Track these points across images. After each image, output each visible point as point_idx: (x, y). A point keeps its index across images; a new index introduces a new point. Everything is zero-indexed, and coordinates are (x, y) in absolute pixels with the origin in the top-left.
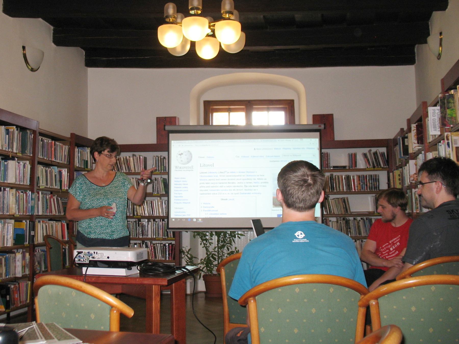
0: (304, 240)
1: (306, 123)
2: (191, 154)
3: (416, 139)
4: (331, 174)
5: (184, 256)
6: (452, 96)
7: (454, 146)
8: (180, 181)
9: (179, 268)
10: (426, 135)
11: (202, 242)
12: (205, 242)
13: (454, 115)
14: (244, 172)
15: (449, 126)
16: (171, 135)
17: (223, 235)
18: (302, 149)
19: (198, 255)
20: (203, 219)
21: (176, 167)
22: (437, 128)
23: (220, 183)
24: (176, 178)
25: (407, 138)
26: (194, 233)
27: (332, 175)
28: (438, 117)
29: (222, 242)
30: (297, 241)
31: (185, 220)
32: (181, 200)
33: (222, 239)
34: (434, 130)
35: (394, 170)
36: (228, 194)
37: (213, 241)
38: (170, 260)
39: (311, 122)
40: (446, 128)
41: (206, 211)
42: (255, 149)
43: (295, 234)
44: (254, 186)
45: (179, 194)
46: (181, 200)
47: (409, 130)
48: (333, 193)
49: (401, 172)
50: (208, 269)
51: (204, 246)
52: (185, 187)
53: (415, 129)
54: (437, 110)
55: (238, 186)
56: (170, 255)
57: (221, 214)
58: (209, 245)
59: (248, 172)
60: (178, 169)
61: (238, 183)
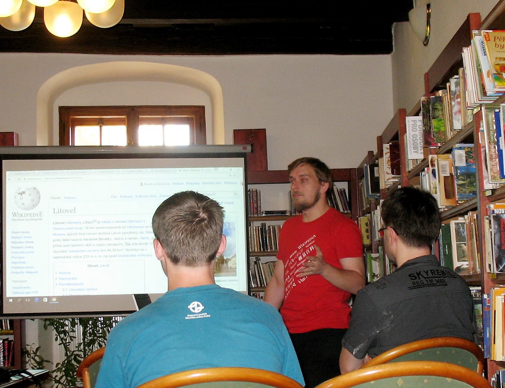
0: (203, 314)
1: (222, 143)
2: (38, 192)
3: (390, 167)
4: (262, 224)
5: (29, 359)
6: (440, 99)
7: (442, 175)
8: (21, 237)
9: (18, 373)
10: (405, 160)
11: (58, 336)
12: (62, 335)
13: (442, 129)
14: (125, 222)
15: (436, 144)
16: (4, 162)
17: (92, 324)
18: (217, 183)
19: (52, 358)
20: (59, 298)
21: (14, 214)
22: (419, 148)
23: (87, 240)
24: (14, 232)
25: (377, 165)
26: (44, 322)
27: (264, 225)
28: (420, 133)
29: (90, 336)
30: (192, 317)
31: (29, 300)
32: (23, 268)
33: (91, 330)
34: (414, 152)
35: (359, 217)
36: (100, 256)
37: (75, 334)
38: (6, 366)
39: (231, 142)
40: (431, 148)
41: (63, 285)
42: (142, 183)
43: (189, 307)
44: (140, 244)
45: (19, 258)
46: (23, 268)
47: (381, 153)
48: (265, 254)
49: (370, 218)
50: (69, 378)
51: (61, 342)
52: (30, 247)
53: (389, 151)
54: (419, 121)
55: (115, 245)
56: (7, 358)
57: (88, 290)
58: (70, 341)
59: (131, 221)
60: (17, 218)
61: (116, 239)
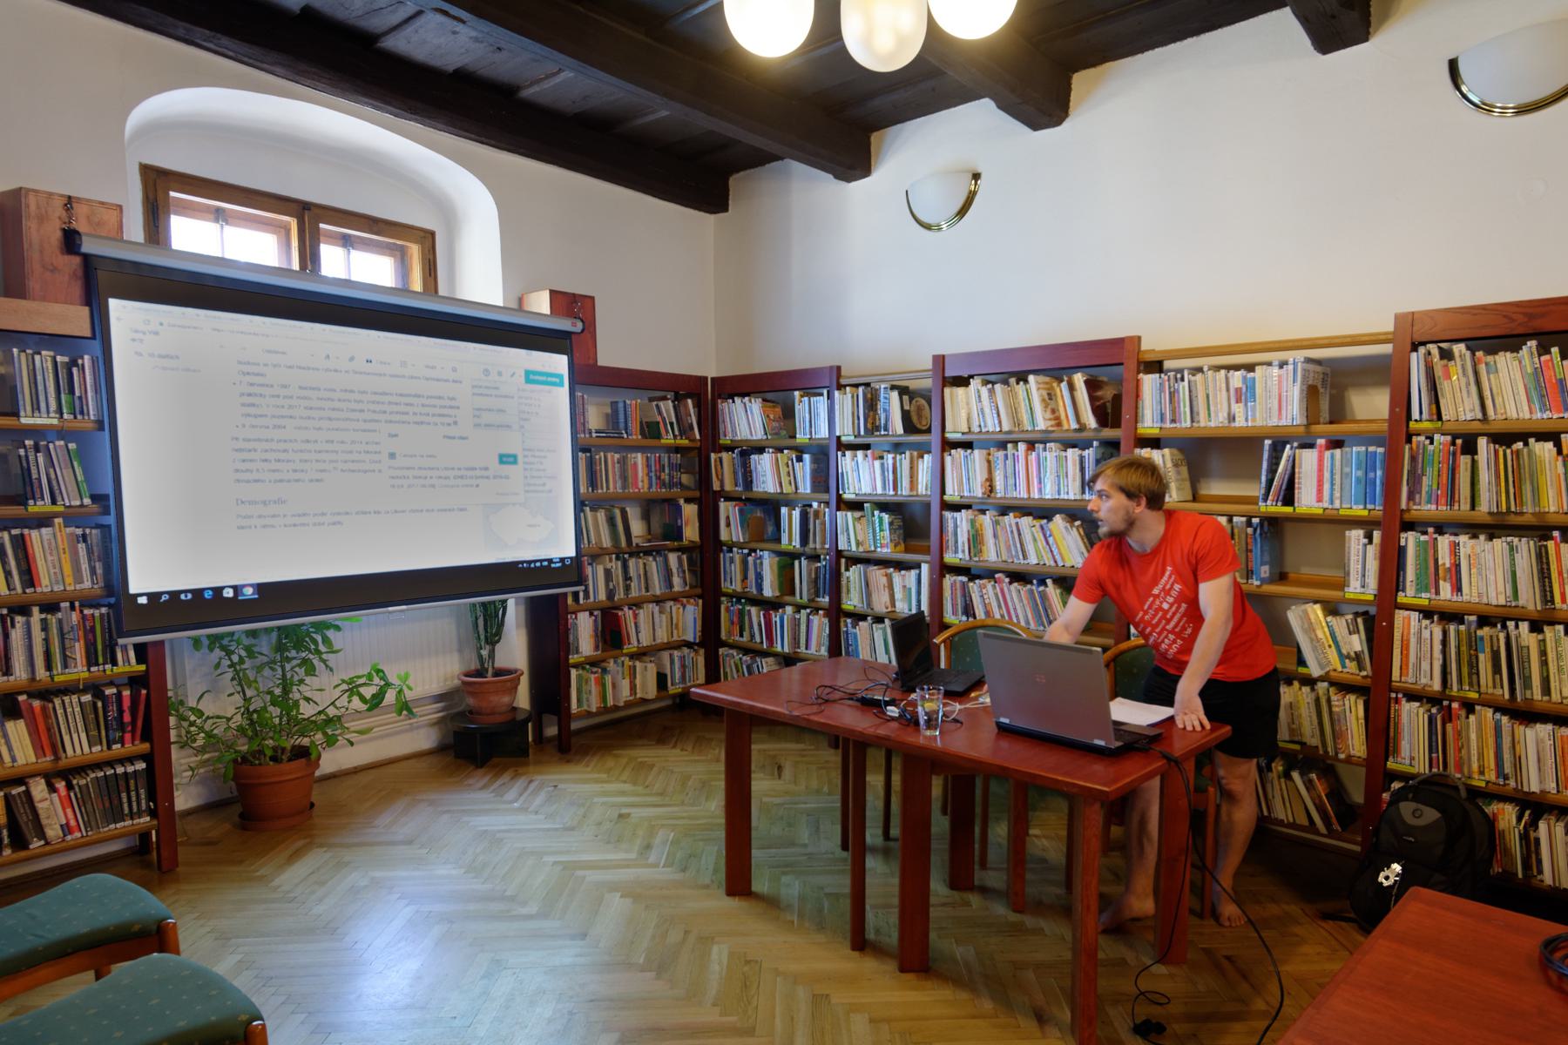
31: (190, 596)
